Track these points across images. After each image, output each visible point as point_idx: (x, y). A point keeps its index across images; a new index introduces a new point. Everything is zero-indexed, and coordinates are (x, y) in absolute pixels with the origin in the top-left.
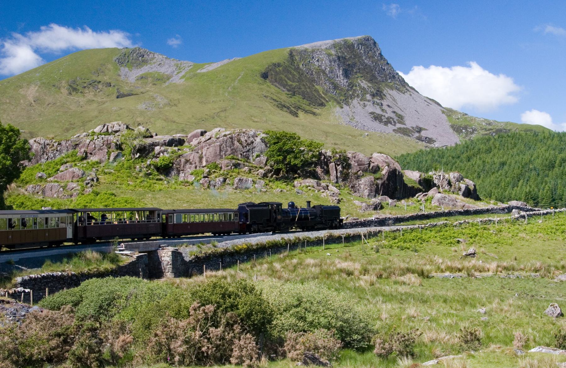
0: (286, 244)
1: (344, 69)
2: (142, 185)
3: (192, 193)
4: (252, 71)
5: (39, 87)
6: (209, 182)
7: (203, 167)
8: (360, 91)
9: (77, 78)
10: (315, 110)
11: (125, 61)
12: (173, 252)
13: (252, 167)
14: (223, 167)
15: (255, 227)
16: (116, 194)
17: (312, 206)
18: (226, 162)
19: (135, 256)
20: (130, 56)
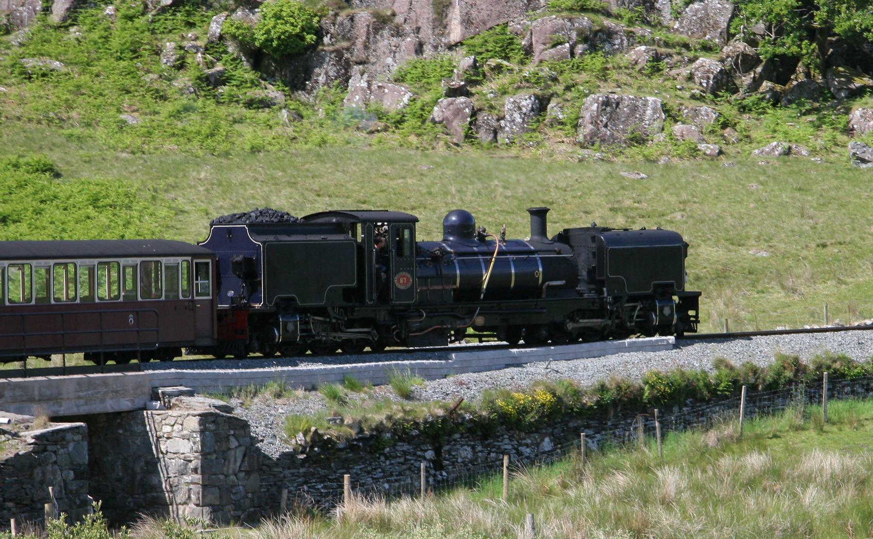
0: (736, 384)
2: (180, 125)
3: (392, 162)
6: (474, 113)
7: (450, 47)
12: (204, 418)
13: (667, 45)
14: (538, 48)
15: (293, 324)
16: (61, 167)
17: (553, 229)
18: (549, 25)
19: (29, 436)
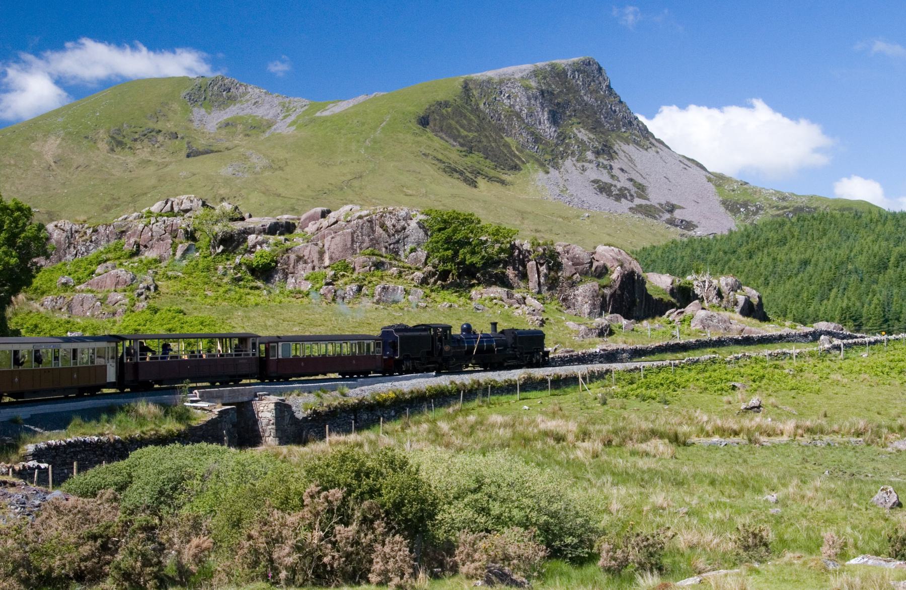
0: (459, 391)
1: (550, 111)
2: (228, 296)
3: (308, 309)
4: (404, 113)
5: (63, 139)
6: (335, 292)
7: (325, 268)
8: (576, 147)
9: (123, 124)
10: (504, 177)
11: (199, 98)
12: (277, 404)
13: (403, 267)
14: (357, 268)
15: (409, 364)
16: (185, 311)
17: (499, 330)
18: (361, 260)
19: (216, 411)
20: (208, 91)
